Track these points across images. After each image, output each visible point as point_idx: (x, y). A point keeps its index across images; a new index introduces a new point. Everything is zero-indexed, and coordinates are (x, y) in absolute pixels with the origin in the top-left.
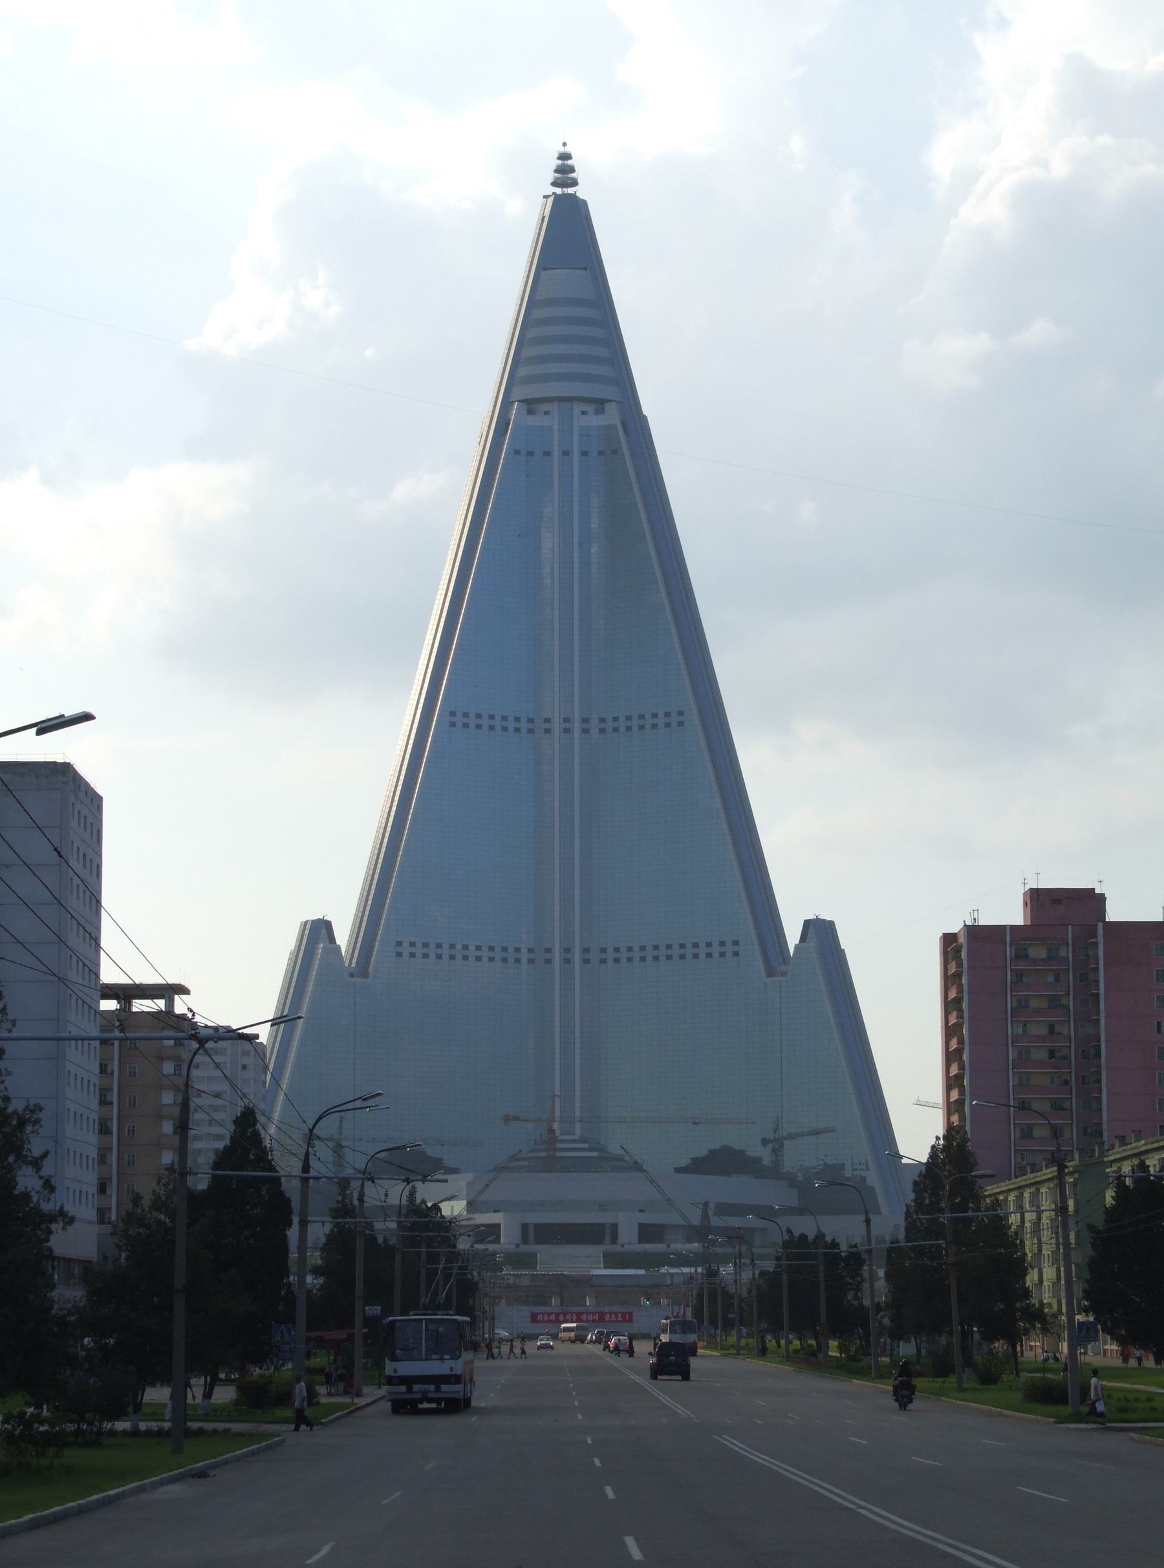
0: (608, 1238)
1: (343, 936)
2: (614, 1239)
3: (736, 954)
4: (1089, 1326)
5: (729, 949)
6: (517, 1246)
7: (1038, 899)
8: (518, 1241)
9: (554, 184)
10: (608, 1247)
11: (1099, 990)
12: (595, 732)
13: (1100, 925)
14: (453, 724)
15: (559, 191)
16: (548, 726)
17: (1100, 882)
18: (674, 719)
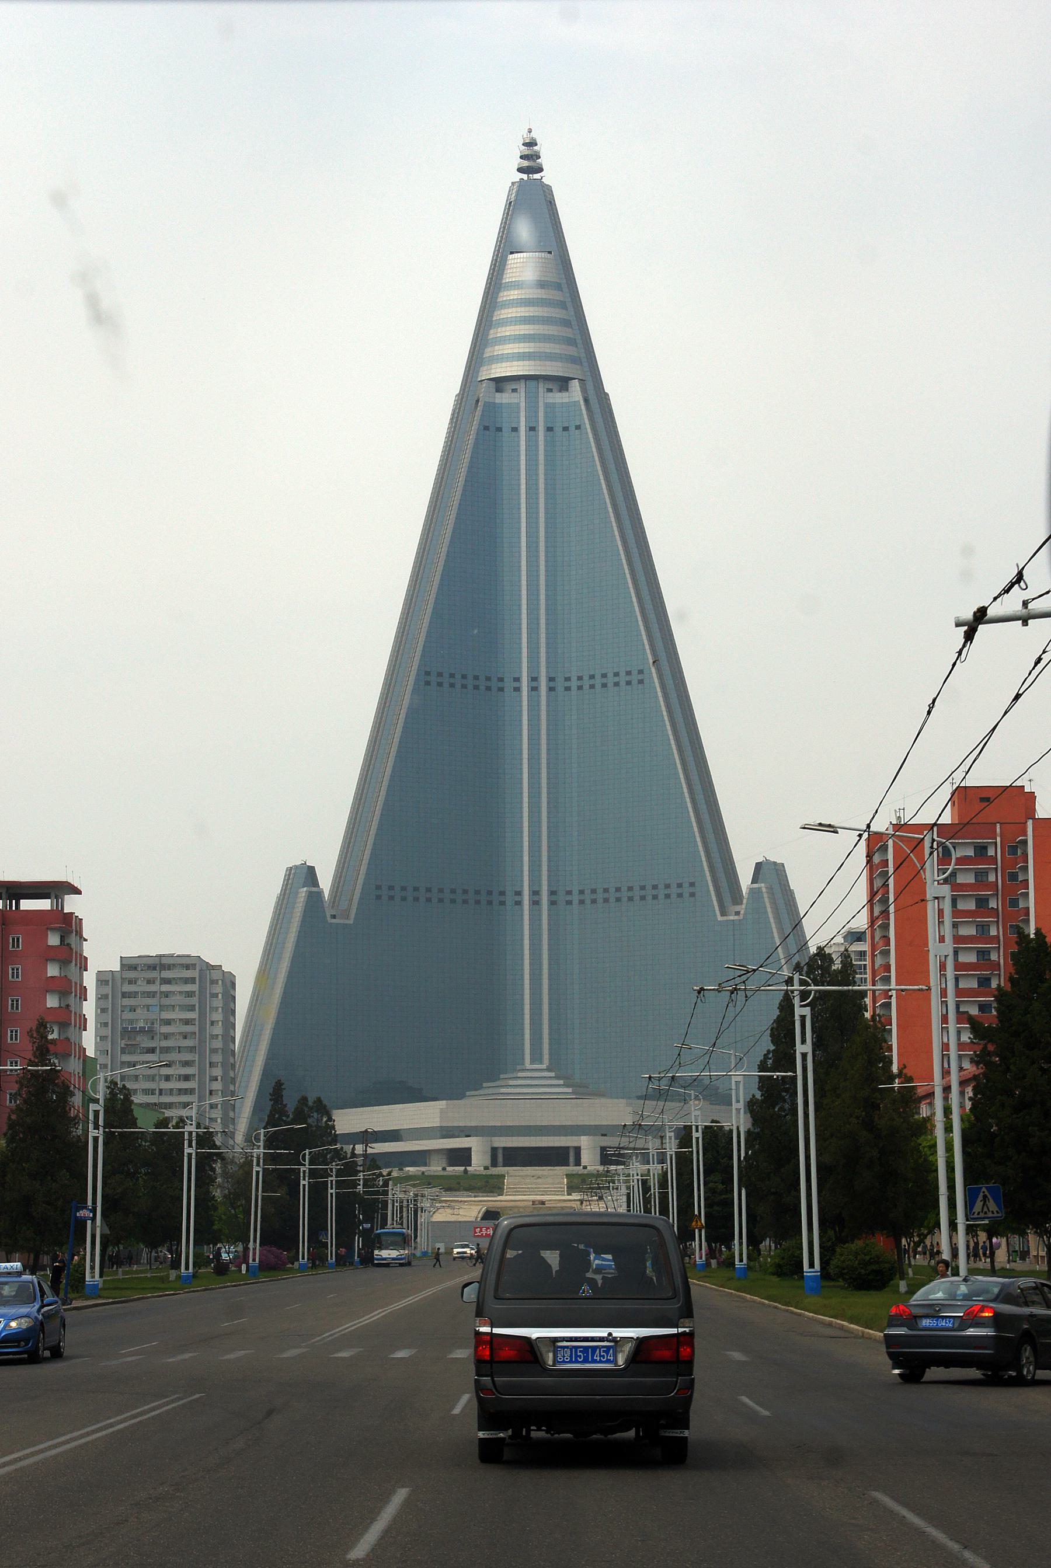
0: (572, 1159)
1: (325, 882)
2: (578, 1163)
3: (692, 895)
4: (986, 1193)
5: (686, 890)
6: (486, 1168)
7: (962, 795)
8: (488, 1163)
9: (520, 170)
10: (572, 1169)
11: (1028, 889)
12: (560, 689)
13: (1030, 823)
14: (428, 683)
15: (525, 177)
16: (516, 684)
17: (1030, 780)
18: (635, 678)
